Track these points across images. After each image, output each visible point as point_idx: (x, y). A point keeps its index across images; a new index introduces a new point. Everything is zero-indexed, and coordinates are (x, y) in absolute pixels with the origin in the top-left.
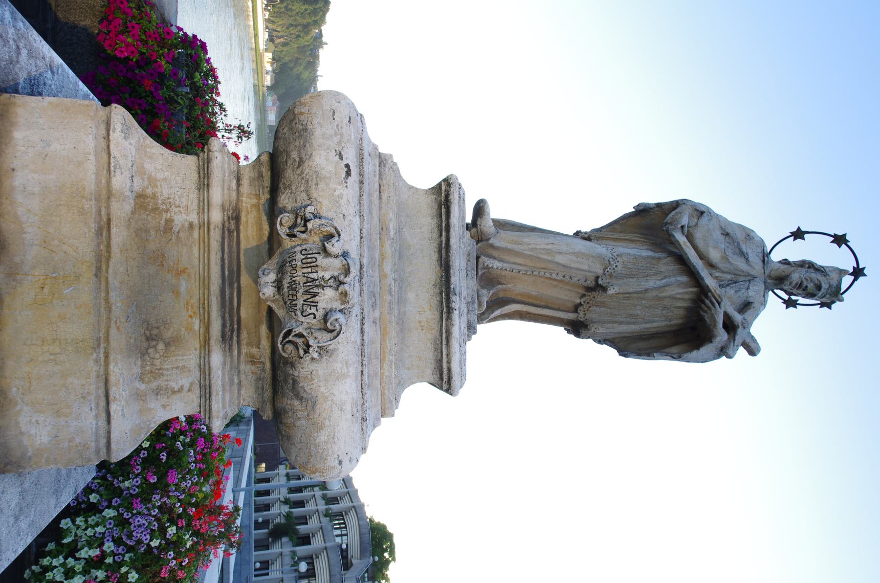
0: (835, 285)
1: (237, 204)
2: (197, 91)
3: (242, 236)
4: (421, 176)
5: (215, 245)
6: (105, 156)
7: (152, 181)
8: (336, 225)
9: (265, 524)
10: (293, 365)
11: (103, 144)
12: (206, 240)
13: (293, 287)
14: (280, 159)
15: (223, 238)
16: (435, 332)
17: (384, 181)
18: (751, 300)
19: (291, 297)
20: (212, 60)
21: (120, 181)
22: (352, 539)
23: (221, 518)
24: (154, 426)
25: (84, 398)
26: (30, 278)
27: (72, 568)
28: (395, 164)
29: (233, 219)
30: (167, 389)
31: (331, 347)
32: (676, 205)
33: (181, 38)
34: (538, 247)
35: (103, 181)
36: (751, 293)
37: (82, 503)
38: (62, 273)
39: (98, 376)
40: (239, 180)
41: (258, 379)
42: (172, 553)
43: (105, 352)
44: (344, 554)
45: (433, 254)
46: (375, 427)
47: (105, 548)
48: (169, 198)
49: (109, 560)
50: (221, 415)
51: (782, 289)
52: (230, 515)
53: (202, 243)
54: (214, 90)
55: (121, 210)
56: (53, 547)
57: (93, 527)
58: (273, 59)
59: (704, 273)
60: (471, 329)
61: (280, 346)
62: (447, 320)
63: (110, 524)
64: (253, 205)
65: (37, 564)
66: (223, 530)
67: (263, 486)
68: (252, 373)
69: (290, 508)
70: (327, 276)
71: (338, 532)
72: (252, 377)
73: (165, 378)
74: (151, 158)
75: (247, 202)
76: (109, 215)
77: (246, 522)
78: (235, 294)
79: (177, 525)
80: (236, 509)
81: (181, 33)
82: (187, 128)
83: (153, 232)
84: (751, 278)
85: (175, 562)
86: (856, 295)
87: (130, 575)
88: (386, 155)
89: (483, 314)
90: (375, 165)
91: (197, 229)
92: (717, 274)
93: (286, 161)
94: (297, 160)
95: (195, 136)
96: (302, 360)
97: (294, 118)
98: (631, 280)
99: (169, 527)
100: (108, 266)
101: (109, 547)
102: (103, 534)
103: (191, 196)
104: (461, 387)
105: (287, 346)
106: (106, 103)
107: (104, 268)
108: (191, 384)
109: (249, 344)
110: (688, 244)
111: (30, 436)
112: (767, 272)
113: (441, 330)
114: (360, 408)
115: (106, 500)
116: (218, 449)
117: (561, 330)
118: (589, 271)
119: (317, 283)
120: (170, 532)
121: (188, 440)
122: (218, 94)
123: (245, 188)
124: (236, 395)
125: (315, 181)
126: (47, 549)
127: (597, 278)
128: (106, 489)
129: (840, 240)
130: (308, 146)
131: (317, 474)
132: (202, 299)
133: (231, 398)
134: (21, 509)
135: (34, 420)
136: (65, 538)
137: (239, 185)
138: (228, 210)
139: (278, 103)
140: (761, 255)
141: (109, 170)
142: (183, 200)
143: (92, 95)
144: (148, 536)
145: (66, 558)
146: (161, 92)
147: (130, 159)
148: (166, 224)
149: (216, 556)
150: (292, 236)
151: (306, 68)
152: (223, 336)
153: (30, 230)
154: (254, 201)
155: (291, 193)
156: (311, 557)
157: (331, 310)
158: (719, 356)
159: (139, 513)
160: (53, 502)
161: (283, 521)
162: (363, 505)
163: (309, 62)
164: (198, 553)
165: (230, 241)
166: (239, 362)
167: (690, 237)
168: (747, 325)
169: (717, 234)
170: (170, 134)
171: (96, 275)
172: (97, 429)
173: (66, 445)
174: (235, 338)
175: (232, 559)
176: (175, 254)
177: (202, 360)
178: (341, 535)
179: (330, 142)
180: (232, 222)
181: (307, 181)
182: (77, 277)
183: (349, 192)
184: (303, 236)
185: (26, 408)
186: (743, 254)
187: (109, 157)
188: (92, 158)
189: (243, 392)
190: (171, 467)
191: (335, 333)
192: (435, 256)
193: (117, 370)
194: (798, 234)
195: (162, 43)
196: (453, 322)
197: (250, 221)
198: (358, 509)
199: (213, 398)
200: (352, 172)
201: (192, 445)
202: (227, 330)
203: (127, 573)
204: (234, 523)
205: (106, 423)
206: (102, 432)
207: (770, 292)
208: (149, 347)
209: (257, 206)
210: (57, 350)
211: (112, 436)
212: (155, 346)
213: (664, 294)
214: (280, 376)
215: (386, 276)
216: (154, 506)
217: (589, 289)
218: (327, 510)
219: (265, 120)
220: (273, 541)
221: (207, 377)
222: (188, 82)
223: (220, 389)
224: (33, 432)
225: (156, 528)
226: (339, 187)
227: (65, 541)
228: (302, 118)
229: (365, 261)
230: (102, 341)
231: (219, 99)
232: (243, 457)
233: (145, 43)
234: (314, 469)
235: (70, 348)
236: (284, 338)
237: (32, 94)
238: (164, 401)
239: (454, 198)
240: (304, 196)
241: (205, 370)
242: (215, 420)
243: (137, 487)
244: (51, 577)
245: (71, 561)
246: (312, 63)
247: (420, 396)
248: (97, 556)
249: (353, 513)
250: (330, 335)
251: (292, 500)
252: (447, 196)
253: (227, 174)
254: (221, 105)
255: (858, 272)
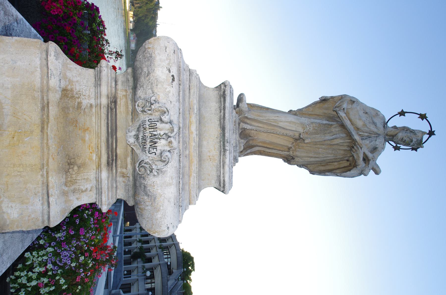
0: (419, 139)
1: (115, 95)
2: (94, 33)
3: (118, 111)
4: (211, 81)
5: (104, 116)
6: (45, 69)
7: (71, 82)
8: (167, 106)
9: (129, 252)
10: (144, 178)
11: (45, 62)
12: (99, 113)
13: (144, 138)
14: (138, 72)
15: (108, 113)
16: (217, 162)
17: (192, 84)
18: (377, 146)
19: (143, 144)
20: (102, 17)
21: (53, 82)
22: (173, 260)
23: (107, 252)
24: (72, 209)
25: (36, 194)
26: (7, 132)
27: (31, 277)
28: (197, 75)
29: (113, 102)
30: (79, 190)
31: (164, 170)
32: (342, 98)
33: (85, 5)
34: (270, 118)
35: (45, 82)
36: (377, 143)
37: (36, 245)
38: (23, 130)
39: (43, 183)
40: (116, 82)
41: (126, 185)
42: (82, 269)
43: (47, 171)
44: (169, 267)
45: (216, 121)
46: (186, 210)
47: (47, 267)
48: (79, 91)
49: (50, 273)
50: (107, 203)
51: (392, 141)
52: (112, 250)
53: (97, 115)
54: (103, 32)
55: (54, 97)
56: (21, 267)
57: (41, 256)
58: (134, 15)
59: (354, 133)
60: (236, 160)
61: (137, 169)
62: (223, 156)
63: (50, 255)
64: (124, 95)
65: (13, 275)
66: (108, 258)
67: (128, 234)
68: (123, 182)
69: (142, 244)
70: (162, 133)
71: (166, 256)
72: (123, 184)
73: (78, 184)
74: (70, 70)
75: (120, 94)
76: (48, 100)
77: (120, 251)
78: (114, 141)
79: (84, 256)
80: (115, 247)
81: (86, 2)
82: (89, 52)
83: (71, 109)
84: (378, 135)
85: (83, 274)
86: (430, 145)
87: (60, 281)
88: (193, 70)
89: (241, 152)
90: (187, 75)
91: (94, 107)
92: (360, 133)
93: (141, 73)
94: (147, 72)
95: (93, 56)
96: (149, 176)
97: (145, 51)
98: (316, 136)
99: (80, 256)
100: (48, 126)
101: (50, 267)
102: (47, 260)
103: (91, 90)
104: (230, 190)
105: (141, 169)
106: (45, 41)
107: (46, 127)
108: (92, 187)
109: (121, 167)
110: (347, 118)
111: (8, 214)
112: (386, 132)
113: (220, 161)
114: (178, 200)
115: (48, 243)
116: (105, 217)
117: (281, 160)
118: (296, 131)
119: (157, 137)
120: (81, 259)
121: (90, 213)
122: (105, 35)
123: (120, 86)
124: (115, 193)
125: (156, 84)
126: (18, 267)
127: (300, 134)
128: (48, 238)
129: (423, 117)
130: (152, 65)
131: (156, 234)
132: (97, 144)
133: (112, 195)
134: (4, 250)
135: (10, 206)
136: (26, 262)
137: (116, 85)
138: (111, 98)
139: (136, 38)
140: (383, 124)
141: (48, 76)
142: (87, 92)
143: (39, 35)
144: (70, 261)
145: (28, 272)
146: (75, 33)
147: (59, 70)
148: (78, 105)
149: (104, 271)
150: (143, 111)
151: (151, 20)
152: (108, 163)
153: (6, 107)
154: (124, 93)
155: (144, 90)
156: (152, 269)
157: (164, 151)
158: (360, 174)
159: (65, 250)
160: (20, 246)
161: (138, 251)
162: (179, 243)
163: (152, 17)
164: (95, 270)
165: (111, 114)
166: (116, 176)
167: (347, 114)
168: (375, 159)
169: (361, 113)
170: (80, 56)
171: (42, 131)
172: (43, 210)
173: (27, 218)
174: (114, 164)
175: (113, 272)
176: (83, 120)
177: (97, 175)
178: (168, 258)
179: (164, 63)
180: (113, 104)
181: (152, 84)
182: (32, 132)
183: (173, 90)
184: (149, 112)
185: (5, 200)
186: (374, 124)
187: (48, 69)
188: (39, 69)
189: (118, 191)
190: (81, 227)
191: (166, 163)
192: (218, 123)
193: (53, 180)
194: (402, 113)
195: (75, 7)
196: (226, 157)
197: (122, 103)
198: (176, 245)
199: (103, 194)
200: (175, 79)
201: (92, 215)
202: (110, 160)
203: (59, 279)
204: (114, 254)
205: (47, 207)
206: (46, 212)
207: (387, 142)
208: (70, 168)
209: (126, 96)
210: (22, 170)
211: (51, 214)
212: (73, 168)
213: (333, 143)
214: (138, 185)
215: (192, 133)
216: (73, 246)
217: (296, 140)
218: (160, 245)
219: (130, 47)
220: (133, 261)
221: (100, 184)
222: (89, 28)
223: (106, 190)
224: (9, 212)
225: (74, 257)
226: (168, 87)
227: (27, 263)
228: (149, 50)
229: (181, 125)
230: (45, 165)
231: (106, 37)
232: (118, 219)
233: (67, 7)
234: (154, 232)
235: (28, 169)
236: (139, 164)
237: (6, 35)
238: (77, 196)
239: (228, 93)
240: (150, 91)
241: (98, 180)
242: (104, 206)
243: (64, 236)
244: (20, 282)
245: (30, 274)
246: (154, 17)
247: (209, 193)
248: (44, 271)
249: (173, 247)
250: (164, 164)
251: (143, 240)
252: (224, 92)
253: (110, 79)
254: (107, 41)
255: (431, 133)
